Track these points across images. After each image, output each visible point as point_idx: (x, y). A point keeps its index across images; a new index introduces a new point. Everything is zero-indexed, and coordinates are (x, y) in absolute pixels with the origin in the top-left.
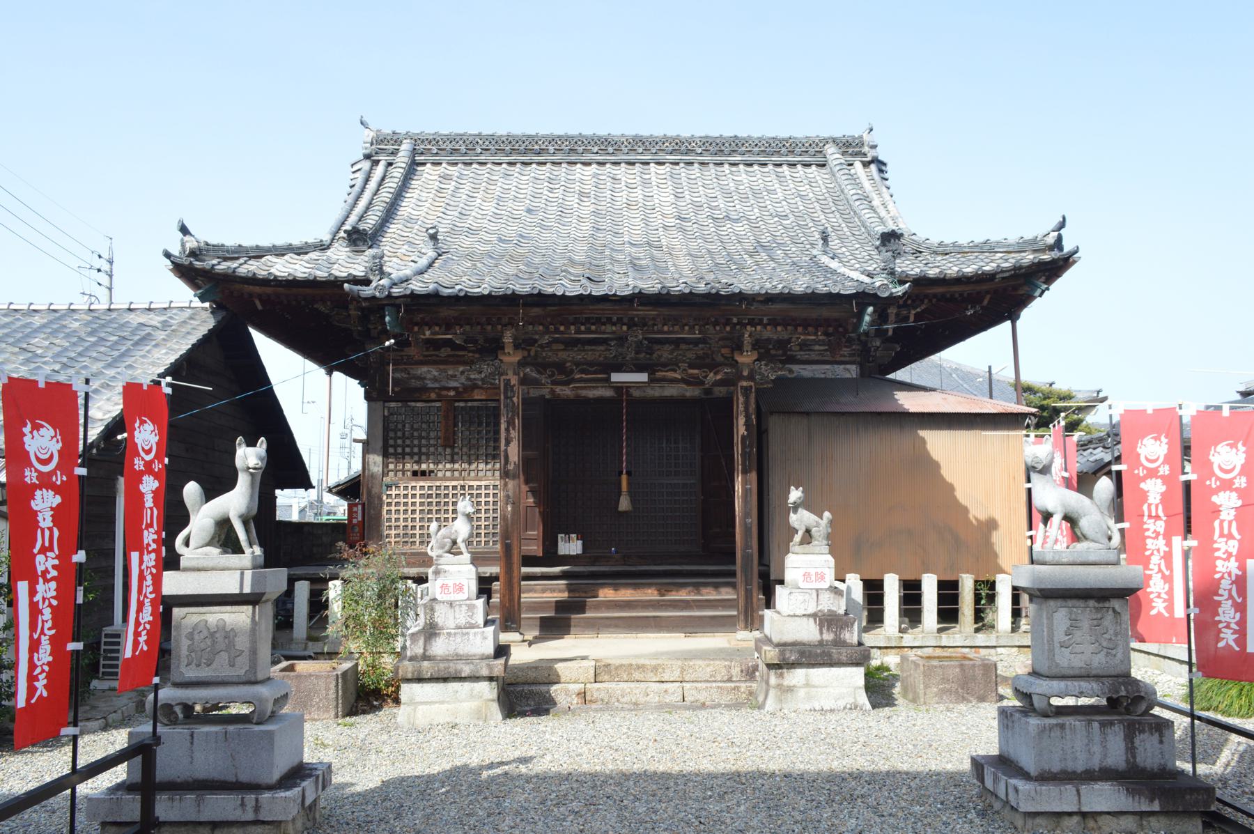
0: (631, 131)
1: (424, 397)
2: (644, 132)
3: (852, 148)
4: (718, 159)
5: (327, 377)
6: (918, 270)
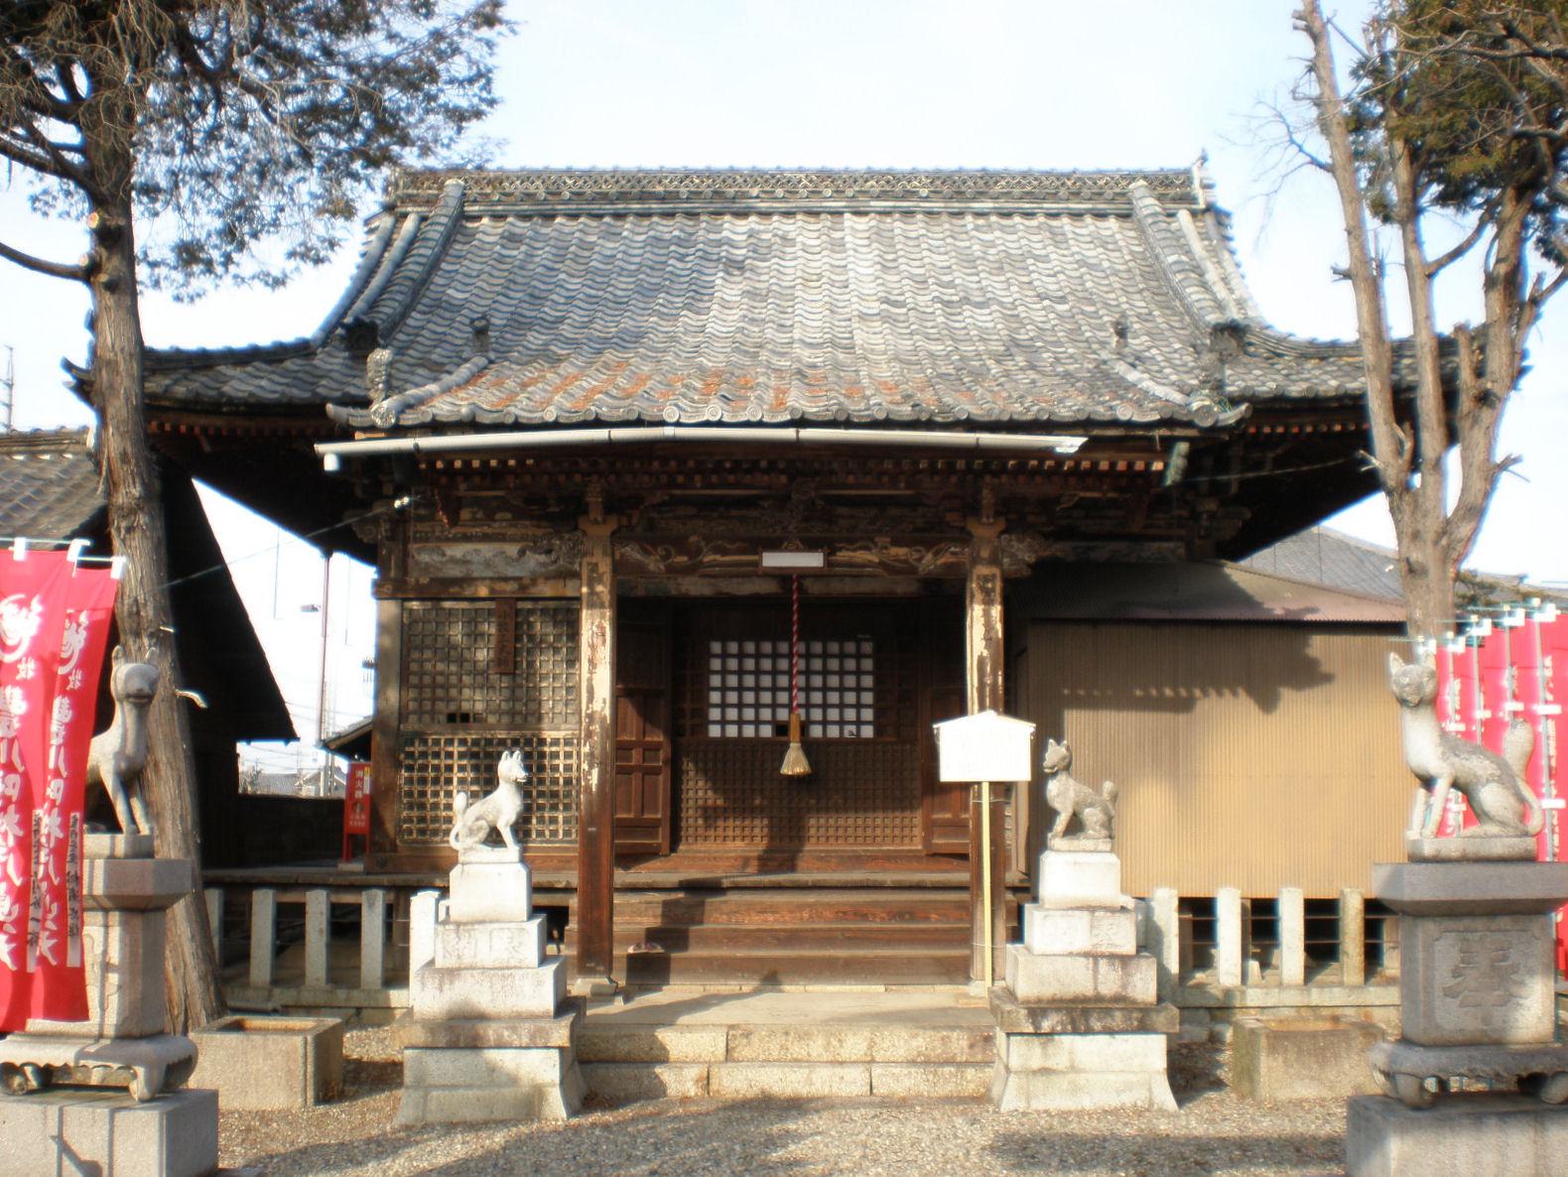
0: (814, 161)
1: (468, 593)
2: (836, 163)
3: (1173, 189)
4: (956, 205)
5: (322, 561)
6: (1273, 385)
